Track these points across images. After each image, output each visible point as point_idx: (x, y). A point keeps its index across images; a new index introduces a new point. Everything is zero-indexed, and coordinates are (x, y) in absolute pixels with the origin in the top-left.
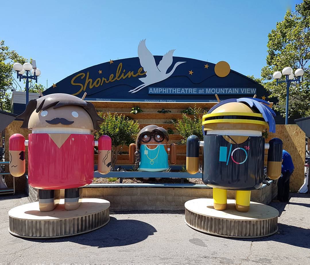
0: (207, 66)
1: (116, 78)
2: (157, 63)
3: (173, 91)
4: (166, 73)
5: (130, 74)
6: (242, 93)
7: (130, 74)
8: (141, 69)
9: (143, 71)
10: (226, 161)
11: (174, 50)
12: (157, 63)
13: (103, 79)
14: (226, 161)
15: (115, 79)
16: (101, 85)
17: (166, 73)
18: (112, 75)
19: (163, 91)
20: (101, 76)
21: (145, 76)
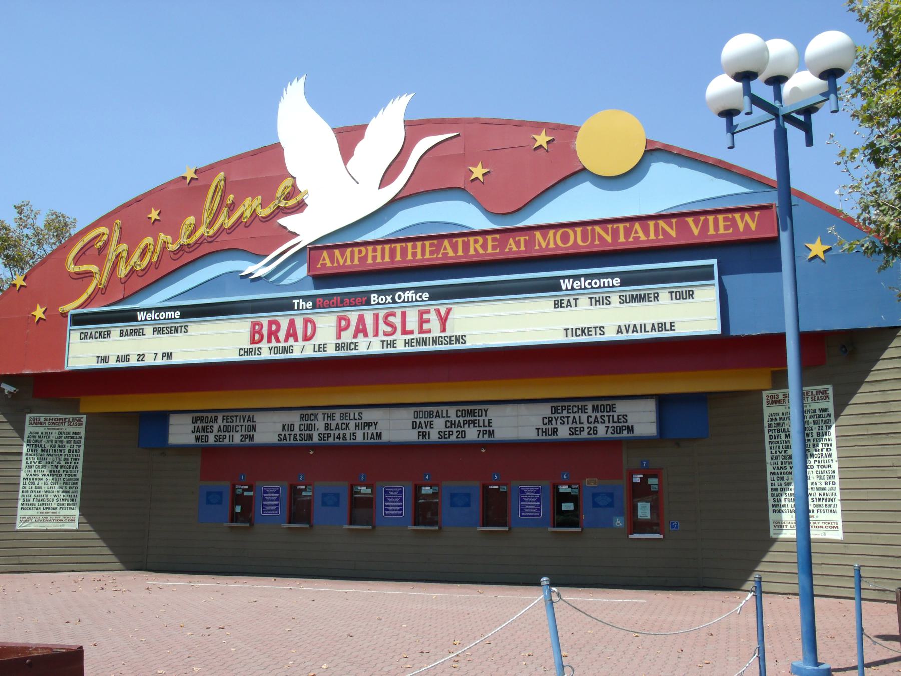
0: (542, 139)
1: (202, 230)
2: (347, 153)
3: (410, 251)
4: (380, 188)
5: (249, 206)
6: (696, 232)
7: (249, 206)
8: (288, 182)
9: (294, 191)
10: (724, 278)
11: (310, 304)
12: (347, 153)
13: (162, 237)
14: (724, 278)
15: (198, 234)
16: (155, 259)
17: (380, 188)
18: (191, 220)
19: (370, 254)
20: (155, 227)
21: (301, 207)
